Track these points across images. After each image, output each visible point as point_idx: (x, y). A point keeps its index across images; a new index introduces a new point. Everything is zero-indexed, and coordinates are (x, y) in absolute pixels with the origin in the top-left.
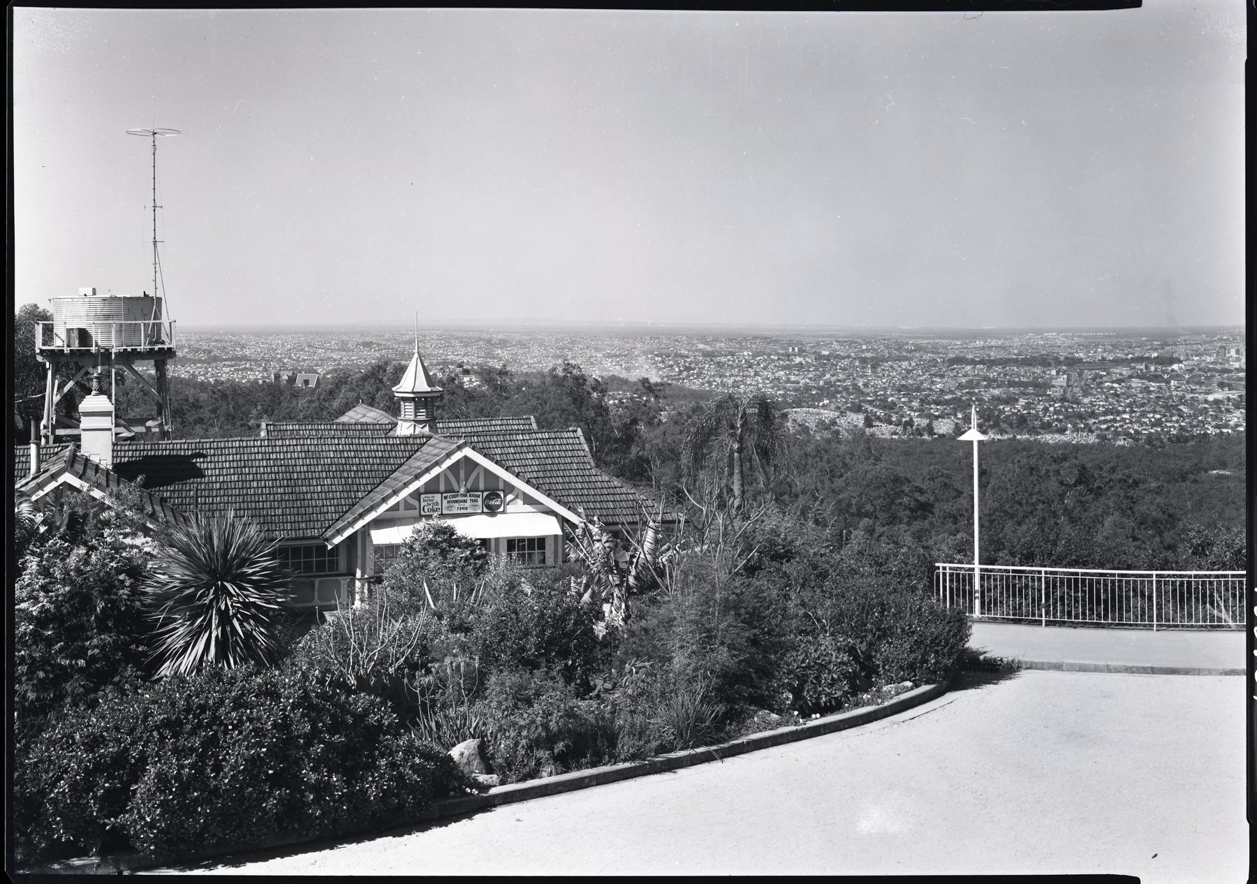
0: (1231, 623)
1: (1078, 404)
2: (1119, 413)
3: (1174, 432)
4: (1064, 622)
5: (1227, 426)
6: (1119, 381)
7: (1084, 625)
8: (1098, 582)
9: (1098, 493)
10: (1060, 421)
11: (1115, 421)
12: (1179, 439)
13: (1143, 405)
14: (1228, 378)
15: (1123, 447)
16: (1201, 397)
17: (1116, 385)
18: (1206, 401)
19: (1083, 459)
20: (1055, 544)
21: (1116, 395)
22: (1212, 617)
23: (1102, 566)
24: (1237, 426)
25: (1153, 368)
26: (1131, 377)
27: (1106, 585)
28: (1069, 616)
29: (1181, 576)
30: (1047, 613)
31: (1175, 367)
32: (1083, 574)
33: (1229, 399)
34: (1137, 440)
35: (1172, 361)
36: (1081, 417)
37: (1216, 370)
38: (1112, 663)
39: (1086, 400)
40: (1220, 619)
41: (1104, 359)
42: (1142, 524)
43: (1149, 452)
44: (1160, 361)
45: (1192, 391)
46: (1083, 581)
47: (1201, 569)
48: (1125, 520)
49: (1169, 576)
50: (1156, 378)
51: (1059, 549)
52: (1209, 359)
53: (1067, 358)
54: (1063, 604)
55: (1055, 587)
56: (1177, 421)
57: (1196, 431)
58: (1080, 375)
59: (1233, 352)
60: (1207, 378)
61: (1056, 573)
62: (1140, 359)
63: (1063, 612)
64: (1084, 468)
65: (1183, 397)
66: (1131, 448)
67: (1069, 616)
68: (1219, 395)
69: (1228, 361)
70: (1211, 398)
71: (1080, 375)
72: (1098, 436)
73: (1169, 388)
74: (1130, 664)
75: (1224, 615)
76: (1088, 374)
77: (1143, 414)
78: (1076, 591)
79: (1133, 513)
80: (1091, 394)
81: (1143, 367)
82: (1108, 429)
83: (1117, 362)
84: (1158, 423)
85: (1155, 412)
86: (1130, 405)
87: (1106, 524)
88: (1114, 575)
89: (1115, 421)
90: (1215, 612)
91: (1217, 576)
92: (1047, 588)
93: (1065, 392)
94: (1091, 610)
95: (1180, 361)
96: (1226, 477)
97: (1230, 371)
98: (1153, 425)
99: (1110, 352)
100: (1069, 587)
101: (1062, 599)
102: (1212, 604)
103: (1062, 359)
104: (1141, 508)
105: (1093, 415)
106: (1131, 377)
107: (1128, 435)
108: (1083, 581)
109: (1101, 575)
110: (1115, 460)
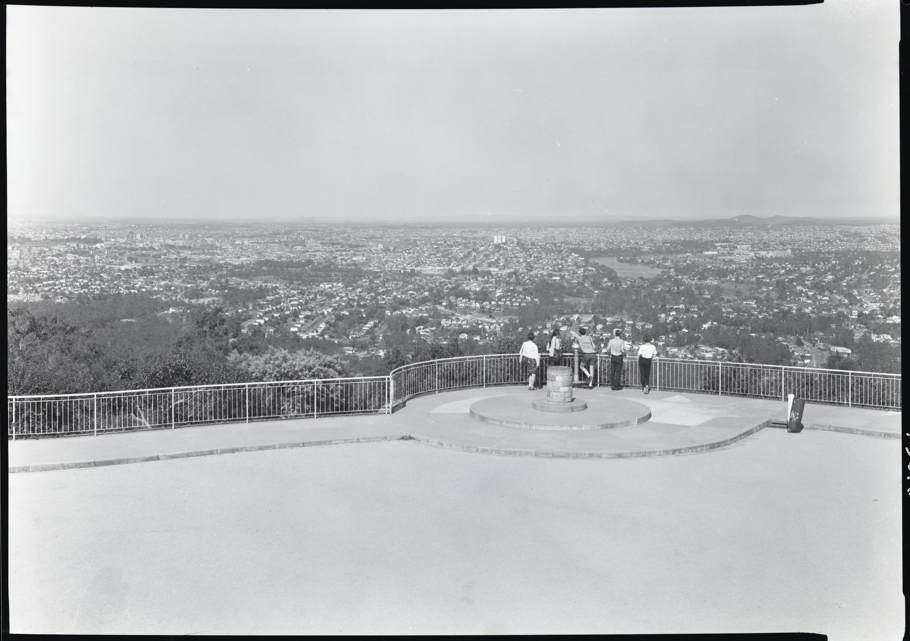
0: (148, 425)
1: (28, 272)
2: (57, 279)
3: (97, 292)
4: (29, 436)
5: (134, 288)
6: (58, 255)
7: (44, 436)
8: (55, 404)
9: (44, 338)
10: (15, 285)
11: (55, 284)
12: (101, 298)
13: (75, 273)
14: (135, 254)
15: (60, 304)
16: (116, 267)
17: (55, 258)
18: (120, 270)
19: (35, 314)
20: (22, 377)
21: (56, 266)
22: (135, 422)
23: (57, 392)
24: (141, 288)
25: (82, 246)
26: (66, 252)
27: (60, 405)
28: (33, 430)
29: (113, 395)
30: (17, 430)
31: (98, 245)
32: (43, 399)
33: (135, 269)
34: (70, 298)
35: (96, 241)
36: (30, 281)
37: (126, 248)
38: (66, 463)
39: (34, 269)
40: (140, 423)
41: (47, 239)
42: (76, 359)
43: (79, 307)
44: (87, 241)
45: (110, 263)
46: (44, 404)
47: (127, 389)
48: (64, 357)
49: (105, 395)
50: (84, 253)
51: (26, 381)
52: (121, 241)
53: (19, 238)
54: (28, 422)
55: (22, 410)
56: (99, 285)
57: (113, 292)
58: (29, 250)
59: (138, 236)
60: (121, 254)
61: (23, 399)
62: (73, 240)
63: (28, 428)
64: (33, 319)
65: (104, 267)
66: (66, 305)
67: (33, 430)
68: (129, 266)
69: (135, 242)
70: (123, 268)
71: (29, 250)
72: (42, 296)
73: (94, 261)
74: (78, 461)
75: (143, 420)
76: (35, 250)
77: (75, 280)
78: (39, 412)
79: (70, 351)
80: (38, 265)
81: (75, 245)
82: (49, 290)
83: (56, 241)
84: (86, 286)
85: (83, 278)
86: (66, 273)
87: (50, 360)
88: (191, 389)
89: (55, 284)
90: (138, 419)
91: (138, 393)
92: (17, 411)
93: (18, 263)
94: (49, 425)
95: (102, 242)
96: (132, 324)
97: (137, 249)
98: (82, 287)
99: (51, 234)
100: (33, 409)
101: (28, 418)
102: (135, 413)
103: (16, 238)
104: (77, 347)
105: (39, 280)
106: (66, 252)
107: (64, 294)
108: (44, 404)
109: (57, 398)
110: (54, 313)
